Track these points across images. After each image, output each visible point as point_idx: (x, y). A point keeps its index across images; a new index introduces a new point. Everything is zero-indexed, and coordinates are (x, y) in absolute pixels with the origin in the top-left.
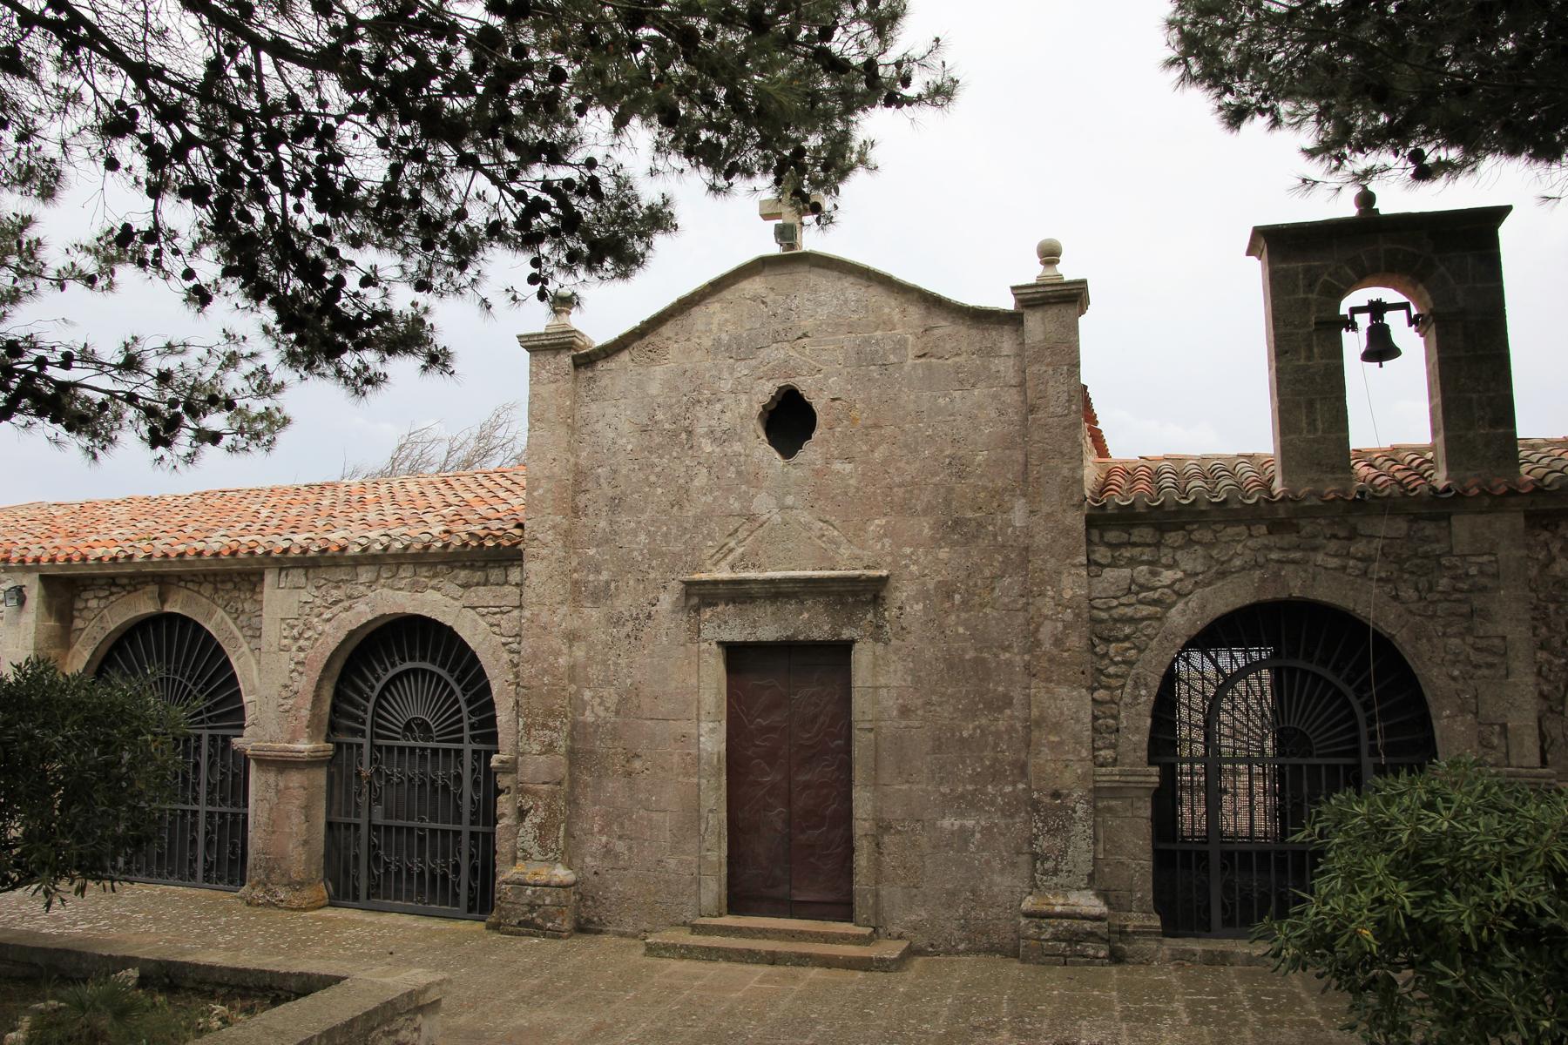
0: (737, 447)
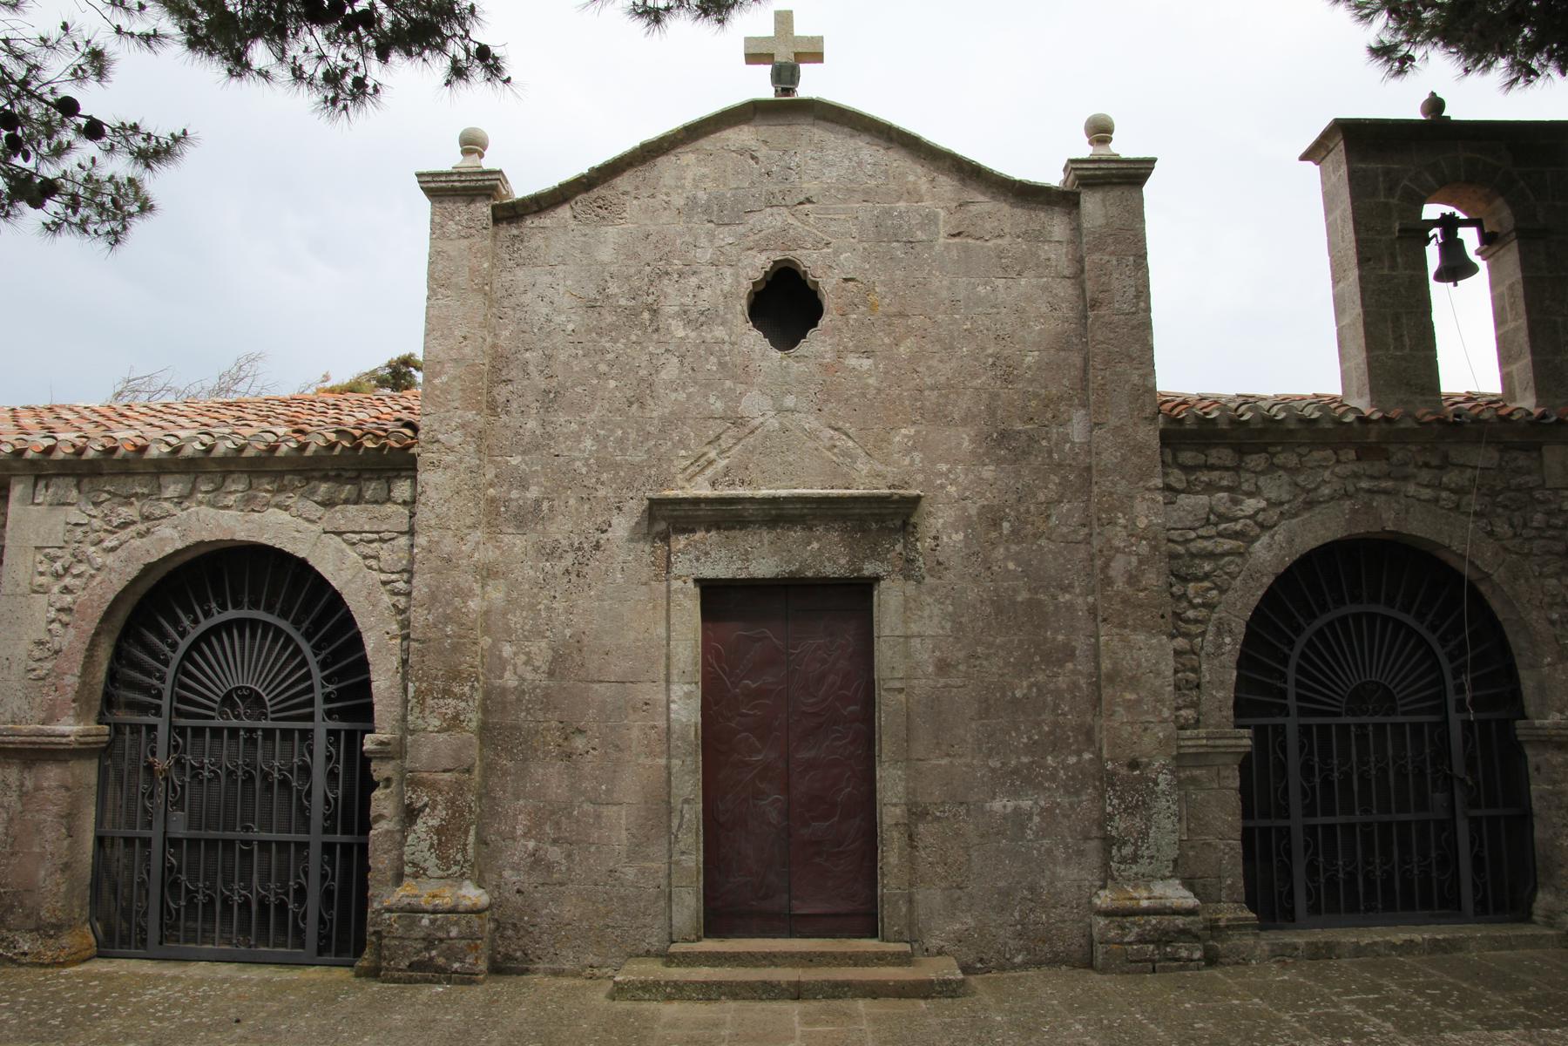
0: (720, 332)
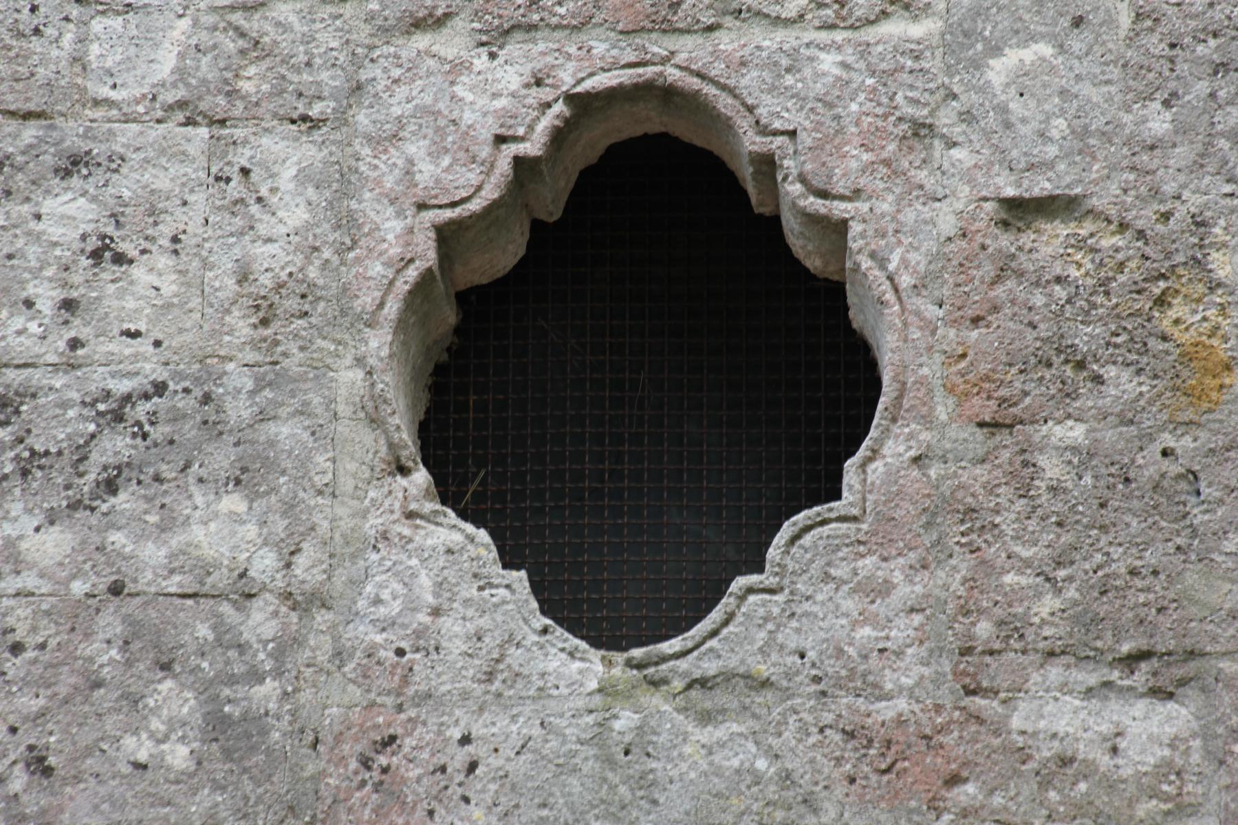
0: (222, 529)
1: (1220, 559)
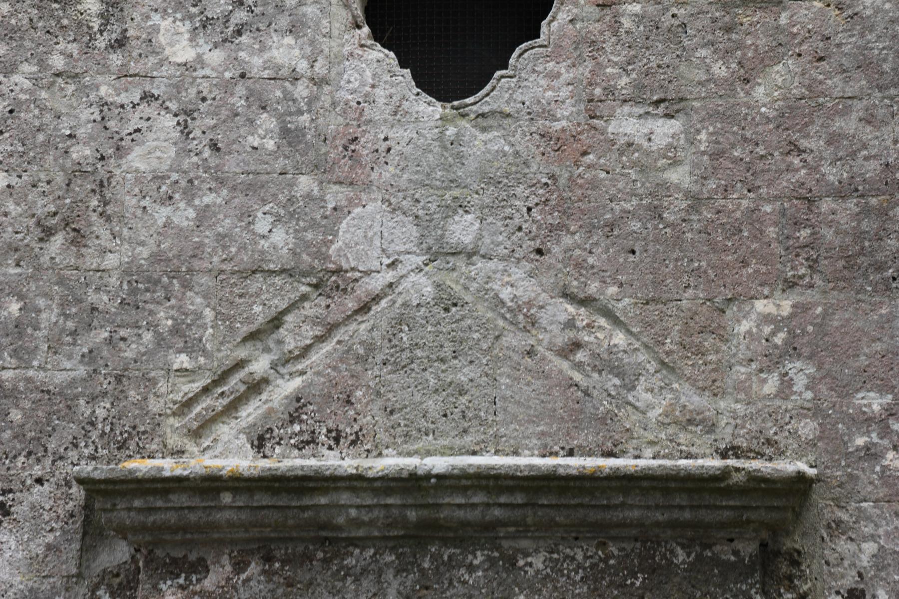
0: (285, 51)
1: (694, 60)
